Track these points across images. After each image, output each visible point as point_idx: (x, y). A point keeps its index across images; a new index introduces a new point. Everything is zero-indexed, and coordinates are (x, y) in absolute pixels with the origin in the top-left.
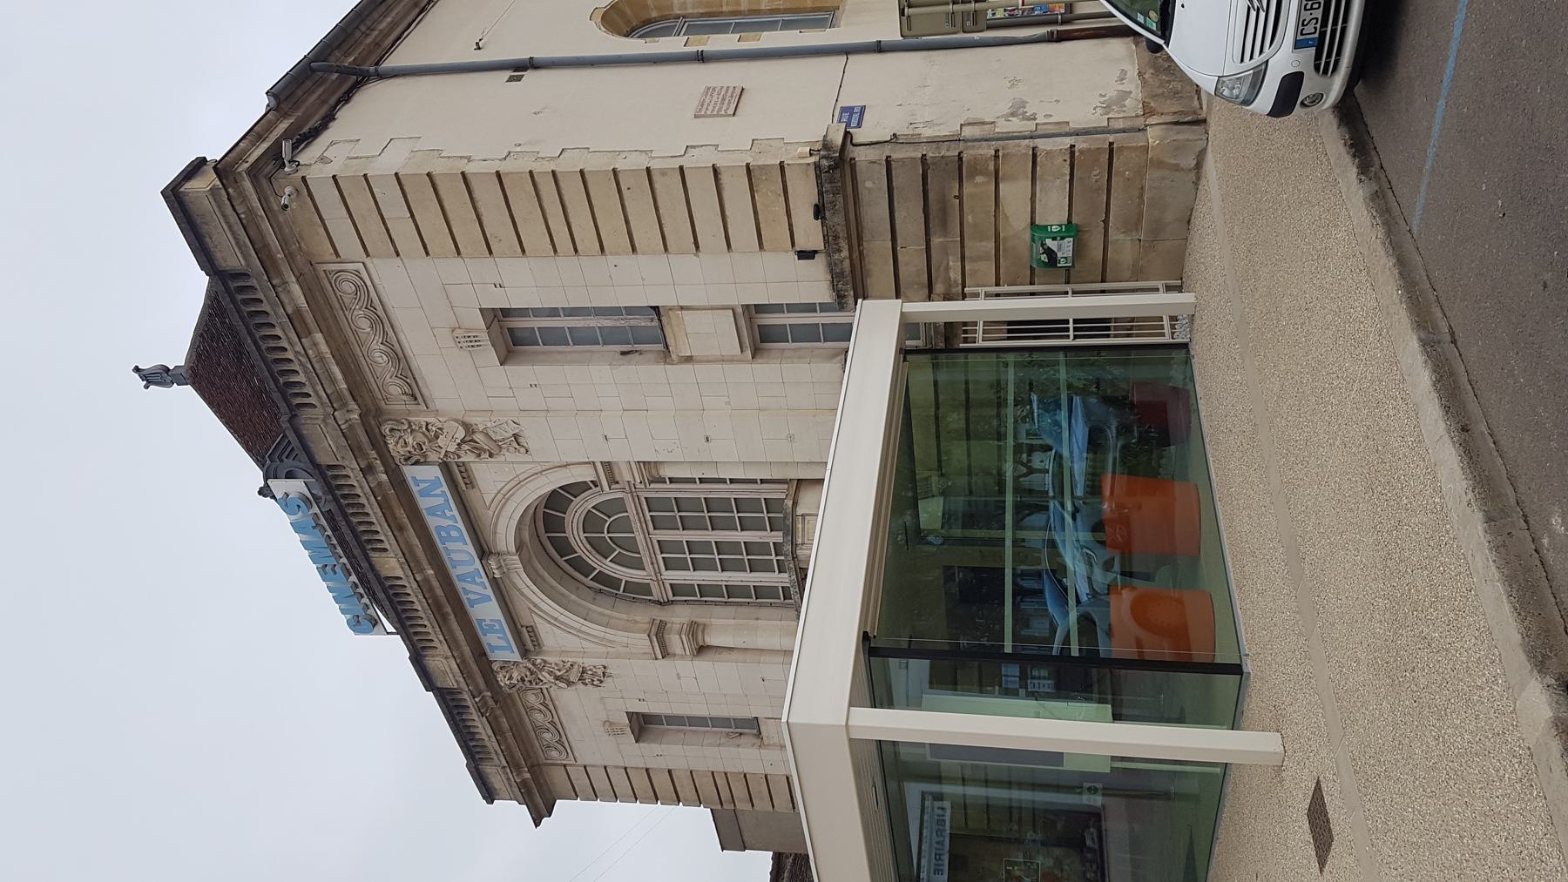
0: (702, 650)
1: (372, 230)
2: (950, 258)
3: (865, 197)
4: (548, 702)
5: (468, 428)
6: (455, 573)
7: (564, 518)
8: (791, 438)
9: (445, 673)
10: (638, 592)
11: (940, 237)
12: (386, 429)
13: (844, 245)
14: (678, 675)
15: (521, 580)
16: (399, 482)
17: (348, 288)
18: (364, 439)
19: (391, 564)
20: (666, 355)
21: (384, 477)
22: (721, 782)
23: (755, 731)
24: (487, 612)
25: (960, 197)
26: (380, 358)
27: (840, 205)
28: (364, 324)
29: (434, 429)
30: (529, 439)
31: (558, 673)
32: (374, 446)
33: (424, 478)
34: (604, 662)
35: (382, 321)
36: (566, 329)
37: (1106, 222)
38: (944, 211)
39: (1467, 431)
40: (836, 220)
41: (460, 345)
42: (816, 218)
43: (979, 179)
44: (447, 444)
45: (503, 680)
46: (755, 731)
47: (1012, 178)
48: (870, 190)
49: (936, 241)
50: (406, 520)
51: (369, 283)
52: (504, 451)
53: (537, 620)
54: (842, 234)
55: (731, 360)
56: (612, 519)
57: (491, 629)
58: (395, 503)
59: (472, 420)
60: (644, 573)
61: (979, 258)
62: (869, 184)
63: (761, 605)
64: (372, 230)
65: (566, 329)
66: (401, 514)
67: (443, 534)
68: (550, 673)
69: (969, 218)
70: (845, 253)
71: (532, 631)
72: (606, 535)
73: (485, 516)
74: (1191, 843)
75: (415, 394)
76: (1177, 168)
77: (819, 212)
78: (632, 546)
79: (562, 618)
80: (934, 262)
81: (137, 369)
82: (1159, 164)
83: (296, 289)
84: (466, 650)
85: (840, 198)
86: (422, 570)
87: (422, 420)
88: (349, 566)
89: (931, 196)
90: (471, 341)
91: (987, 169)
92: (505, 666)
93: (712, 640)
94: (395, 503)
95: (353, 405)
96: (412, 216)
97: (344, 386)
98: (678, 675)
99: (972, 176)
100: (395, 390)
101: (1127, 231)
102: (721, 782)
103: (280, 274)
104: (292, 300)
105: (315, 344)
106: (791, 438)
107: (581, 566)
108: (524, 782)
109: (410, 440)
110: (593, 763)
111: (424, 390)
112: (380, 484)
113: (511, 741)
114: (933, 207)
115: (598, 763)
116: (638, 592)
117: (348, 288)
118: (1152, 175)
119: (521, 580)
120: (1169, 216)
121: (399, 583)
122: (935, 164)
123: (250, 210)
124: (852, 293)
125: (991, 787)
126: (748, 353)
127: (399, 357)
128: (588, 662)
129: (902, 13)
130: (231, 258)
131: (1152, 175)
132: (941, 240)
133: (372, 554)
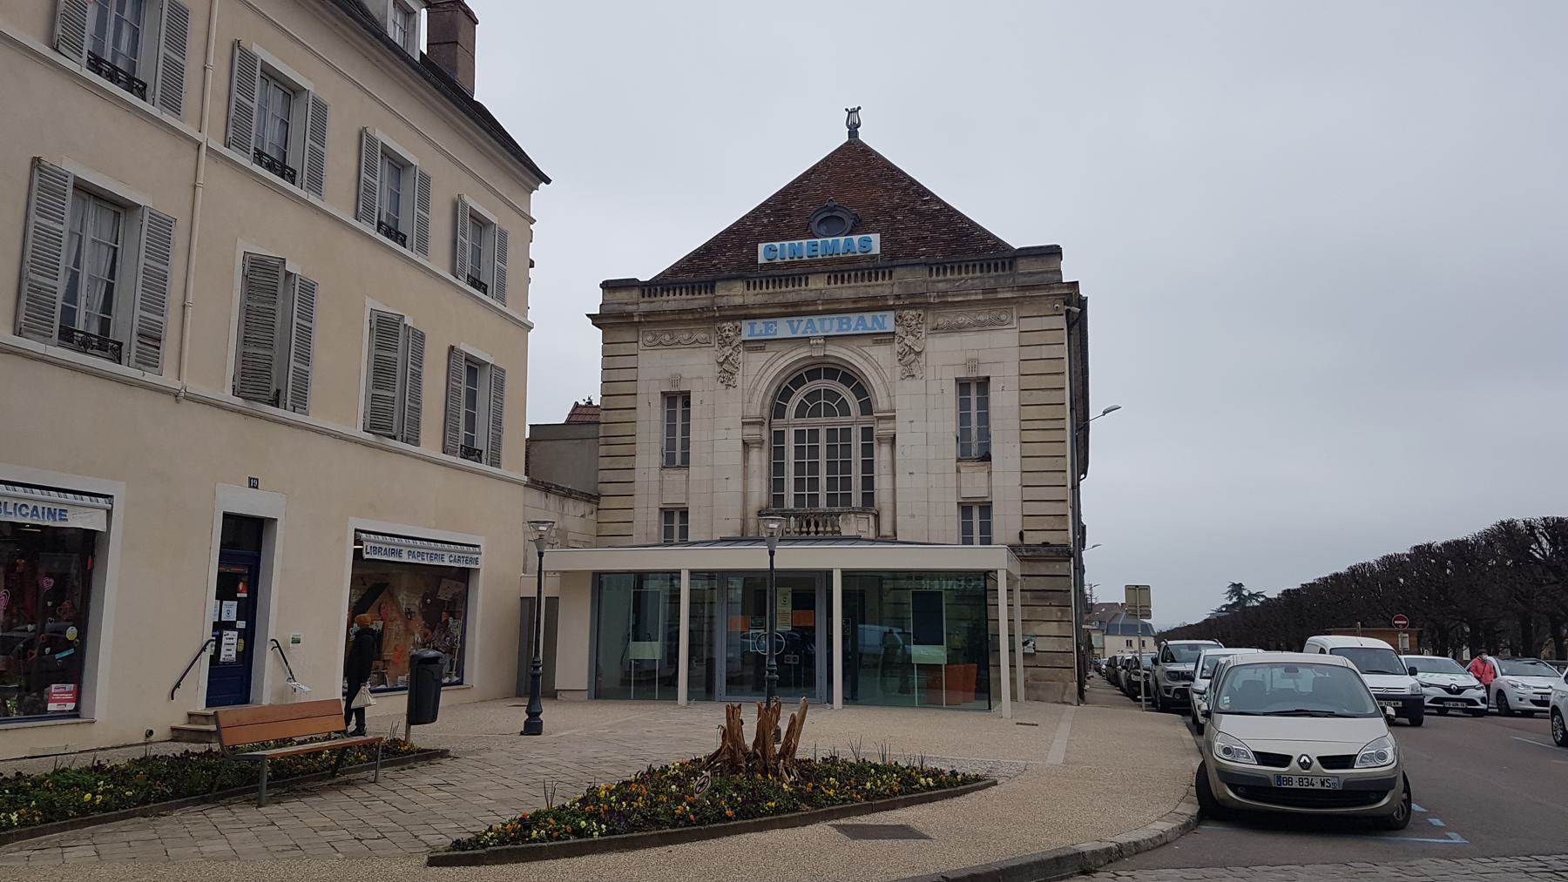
0: (746, 445)
1: (1035, 338)
3: (1051, 565)
4: (697, 345)
5: (919, 354)
6: (815, 318)
8: (913, 516)
9: (730, 290)
10: (778, 411)
12: (920, 312)
13: (1030, 554)
14: (729, 429)
15: (803, 352)
16: (891, 308)
17: (1003, 317)
18: (917, 300)
19: (818, 284)
20: (959, 460)
21: (891, 303)
22: (628, 440)
23: (664, 465)
24: (783, 328)
25: (1050, 605)
26: (961, 319)
27: (1050, 554)
28: (981, 318)
30: (908, 383)
31: (730, 359)
32: (911, 304)
33: (888, 322)
34: (739, 387)
35: (982, 326)
36: (380, 143)
37: (1037, 666)
38: (1044, 598)
40: (1043, 552)
43: (1059, 614)
44: (910, 340)
45: (728, 325)
46: (664, 465)
47: (1059, 627)
48: (1054, 567)
50: (859, 306)
51: (1005, 327)
52: (902, 367)
53: (771, 354)
54: (1036, 554)
55: (959, 492)
57: (767, 328)
58: (871, 303)
59: (923, 355)
60: (793, 417)
62: (1057, 567)
63: (769, 480)
64: (1035, 338)
65: (380, 143)
66: (865, 304)
67: (844, 321)
68: (731, 354)
69: (1040, 609)
70: (1025, 554)
71: (762, 349)
73: (854, 344)
75: (936, 329)
76: (1064, 694)
77: (1045, 544)
78: (815, 413)
79: (771, 369)
81: (859, 108)
82: (1065, 688)
83: (1009, 295)
84: (754, 312)
85: (1054, 555)
86: (822, 304)
87: (923, 330)
88: (815, 258)
89: (1050, 593)
92: (739, 331)
93: (754, 454)
94: (871, 303)
95: (937, 301)
97: (950, 300)
98: (729, 429)
100: (940, 321)
101: (1031, 675)
102: (628, 440)
103: (1018, 291)
104: (1003, 292)
105: (976, 294)
106: (913, 516)
107: (798, 382)
108: (633, 316)
109: (914, 323)
110: (639, 359)
111: (938, 335)
112: (887, 300)
113: (671, 317)
114: (1046, 594)
115: (639, 363)
116: (778, 411)
117: (1003, 317)
118: (1061, 685)
119: (803, 352)
120: (1040, 692)
121: (803, 284)
123: (1053, 288)
125: (670, 607)
126: (961, 501)
127: (960, 328)
128: (738, 377)
129: (1137, 586)
130: (1023, 266)
131: (1061, 685)
133: (827, 275)
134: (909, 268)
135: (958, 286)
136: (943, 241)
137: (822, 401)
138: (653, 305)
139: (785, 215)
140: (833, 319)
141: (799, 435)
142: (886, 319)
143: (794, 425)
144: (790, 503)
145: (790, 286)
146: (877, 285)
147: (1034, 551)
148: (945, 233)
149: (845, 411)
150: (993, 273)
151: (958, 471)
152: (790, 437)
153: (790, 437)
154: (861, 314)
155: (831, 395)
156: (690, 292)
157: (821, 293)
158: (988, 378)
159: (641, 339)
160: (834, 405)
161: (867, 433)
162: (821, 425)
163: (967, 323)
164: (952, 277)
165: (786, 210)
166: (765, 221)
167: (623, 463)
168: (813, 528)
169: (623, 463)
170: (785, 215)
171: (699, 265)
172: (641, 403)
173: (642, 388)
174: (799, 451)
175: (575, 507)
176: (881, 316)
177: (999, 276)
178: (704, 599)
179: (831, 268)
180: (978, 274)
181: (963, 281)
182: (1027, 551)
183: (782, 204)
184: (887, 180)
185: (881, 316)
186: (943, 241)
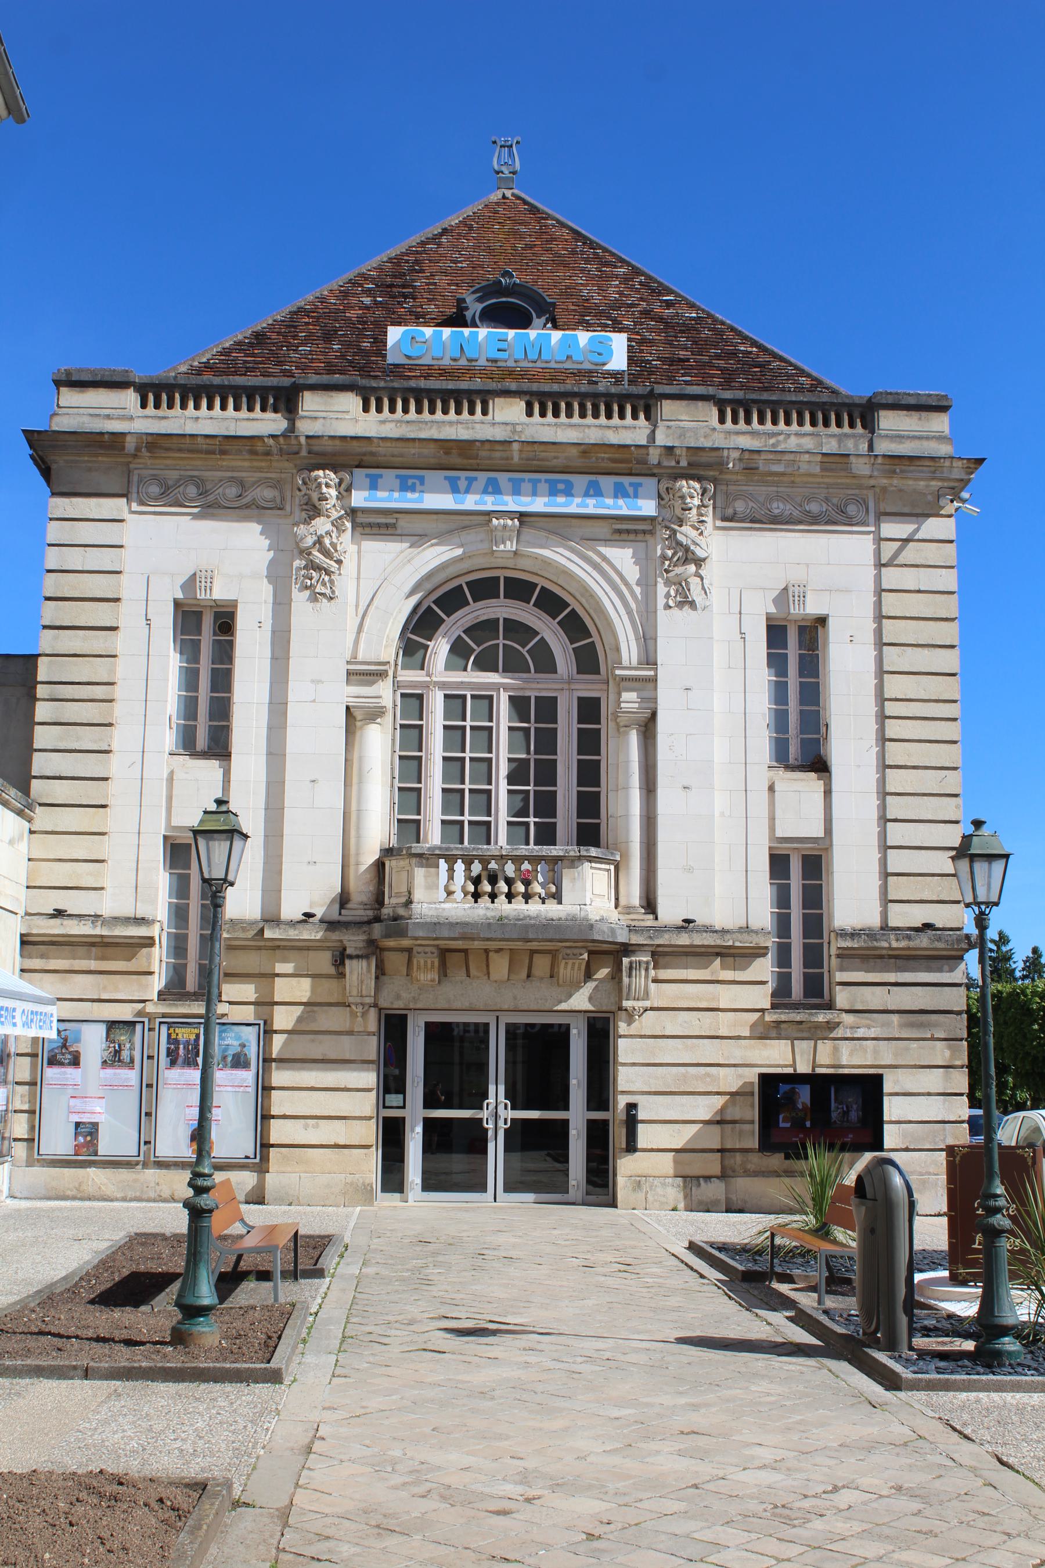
2: (878, 1029)
7: (528, 603)
8: (690, 870)
11: (898, 1021)
22: (99, 692)
25: (933, 1039)
29: (702, 528)
38: (921, 1025)
39: (162, 1521)
41: (796, 586)
42: (923, 925)
49: (895, 1018)
55: (772, 828)
56: (481, 648)
61: (876, 1051)
70: (895, 944)
72: (501, 641)
74: (441, 1329)
77: (928, 926)
80: (875, 1015)
90: (799, 596)
91: (956, 1059)
96: (919, 591)
99: (949, 1048)
102: (99, 692)
122: (29, 926)
124: (856, 946)
132: (896, 1023)
134: (684, 403)
135: (773, 445)
136: (718, 368)
137: (501, 641)
138: (164, 423)
139: (405, 296)
140: (540, 481)
141: (455, 702)
142: (640, 489)
143: (442, 685)
144: (433, 836)
145: (439, 412)
146: (609, 427)
147: (909, 938)
148: (718, 357)
149: (545, 662)
150: (833, 429)
151: (771, 789)
152: (436, 703)
153: (436, 703)
154: (593, 477)
155: (517, 629)
156: (244, 406)
157: (514, 432)
158: (822, 621)
159: (134, 489)
160: (524, 651)
161: (589, 710)
162: (497, 687)
163: (787, 513)
164: (761, 427)
165: (404, 286)
166: (367, 300)
167: (87, 738)
168: (503, 886)
169: (87, 738)
170: (405, 296)
171: (246, 362)
172: (128, 615)
173: (129, 587)
174: (454, 734)
175: (363, 941)
176: (631, 484)
177: (846, 435)
178: (649, 1210)
179: (535, 387)
180: (808, 427)
181: (781, 438)
182: (897, 940)
183: (394, 276)
184: (587, 261)
185: (631, 484)
186: (718, 368)
